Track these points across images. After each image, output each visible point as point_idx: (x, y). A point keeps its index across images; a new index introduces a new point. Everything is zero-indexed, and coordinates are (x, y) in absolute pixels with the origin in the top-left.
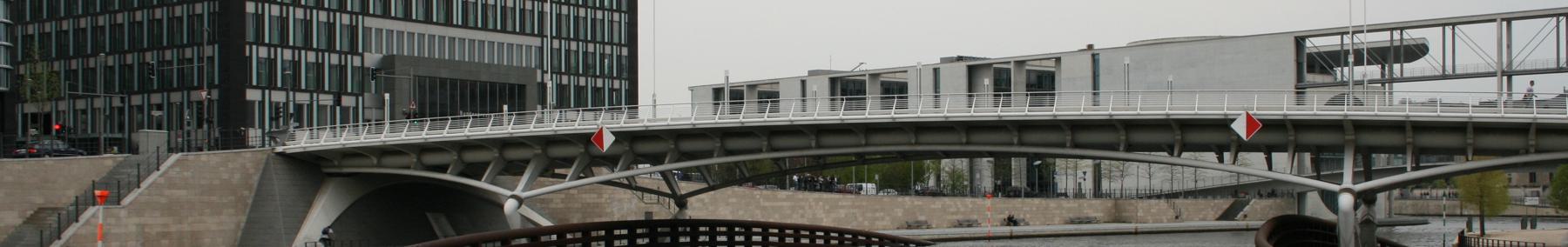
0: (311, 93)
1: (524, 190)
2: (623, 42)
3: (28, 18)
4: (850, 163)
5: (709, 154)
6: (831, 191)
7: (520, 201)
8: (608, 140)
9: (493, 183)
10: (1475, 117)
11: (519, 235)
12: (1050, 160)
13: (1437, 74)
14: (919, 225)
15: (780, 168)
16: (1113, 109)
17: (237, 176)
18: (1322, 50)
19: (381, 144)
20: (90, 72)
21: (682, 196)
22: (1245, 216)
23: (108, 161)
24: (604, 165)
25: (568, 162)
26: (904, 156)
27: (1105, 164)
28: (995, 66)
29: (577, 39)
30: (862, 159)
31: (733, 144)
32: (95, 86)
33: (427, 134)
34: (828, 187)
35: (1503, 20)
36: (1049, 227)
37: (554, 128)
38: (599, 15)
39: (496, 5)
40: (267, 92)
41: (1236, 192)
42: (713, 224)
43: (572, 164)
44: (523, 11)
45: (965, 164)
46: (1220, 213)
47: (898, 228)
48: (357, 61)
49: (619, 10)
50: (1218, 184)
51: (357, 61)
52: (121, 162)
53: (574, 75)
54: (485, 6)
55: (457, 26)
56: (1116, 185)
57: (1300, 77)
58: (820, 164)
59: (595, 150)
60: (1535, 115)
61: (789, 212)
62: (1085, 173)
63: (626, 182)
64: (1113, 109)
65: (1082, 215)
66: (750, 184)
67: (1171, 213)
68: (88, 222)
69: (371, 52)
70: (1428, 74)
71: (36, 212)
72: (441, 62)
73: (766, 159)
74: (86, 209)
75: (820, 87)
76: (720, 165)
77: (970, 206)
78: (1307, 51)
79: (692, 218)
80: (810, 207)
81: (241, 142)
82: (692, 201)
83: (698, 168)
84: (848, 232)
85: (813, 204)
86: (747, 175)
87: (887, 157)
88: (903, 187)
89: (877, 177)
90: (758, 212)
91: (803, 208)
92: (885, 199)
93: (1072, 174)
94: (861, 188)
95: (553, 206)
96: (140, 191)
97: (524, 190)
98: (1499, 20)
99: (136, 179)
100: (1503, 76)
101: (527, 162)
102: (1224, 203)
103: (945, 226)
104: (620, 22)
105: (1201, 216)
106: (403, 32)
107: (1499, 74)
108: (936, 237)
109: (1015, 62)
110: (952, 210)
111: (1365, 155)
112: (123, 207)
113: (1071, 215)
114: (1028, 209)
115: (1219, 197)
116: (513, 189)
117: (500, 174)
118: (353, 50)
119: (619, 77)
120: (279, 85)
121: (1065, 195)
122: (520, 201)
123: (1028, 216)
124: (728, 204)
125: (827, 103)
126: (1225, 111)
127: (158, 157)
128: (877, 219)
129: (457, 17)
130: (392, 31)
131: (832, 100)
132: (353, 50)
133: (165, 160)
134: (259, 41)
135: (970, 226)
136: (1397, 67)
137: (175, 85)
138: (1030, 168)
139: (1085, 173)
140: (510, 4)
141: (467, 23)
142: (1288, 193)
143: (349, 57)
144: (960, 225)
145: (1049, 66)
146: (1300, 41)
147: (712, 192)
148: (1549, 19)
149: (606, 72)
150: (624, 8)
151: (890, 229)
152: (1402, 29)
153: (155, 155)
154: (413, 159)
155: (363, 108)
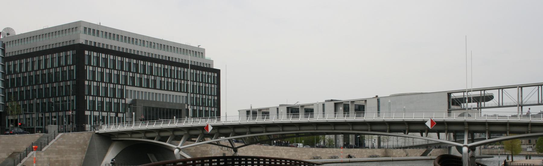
0: (108, 112)
1: (181, 146)
2: (215, 95)
3: (10, 87)
4: (294, 136)
5: (245, 134)
6: (287, 146)
7: (180, 150)
8: (210, 128)
9: (170, 143)
11: (179, 161)
12: (363, 135)
13: (497, 106)
14: (317, 158)
17: (82, 141)
20: (31, 105)
21: (236, 148)
22: (430, 155)
23: (37, 136)
24: (209, 137)
25: (196, 136)
26: (313, 134)
27: (382, 137)
28: (344, 103)
30: (298, 135)
32: (33, 110)
34: (286, 145)
35: (519, 87)
36: (362, 159)
38: (207, 85)
40: (92, 112)
41: (427, 147)
42: (246, 158)
45: (333, 137)
46: (422, 154)
48: (123, 101)
49: (214, 84)
50: (421, 144)
51: (123, 101)
52: (42, 136)
53: (198, 106)
55: (158, 89)
56: (386, 144)
58: (283, 137)
59: (206, 132)
62: (375, 140)
63: (216, 143)
65: (374, 155)
66: (259, 144)
67: (405, 154)
68: (30, 157)
69: (128, 98)
72: (152, 101)
74: (30, 152)
76: (249, 137)
78: (452, 98)
80: (280, 152)
81: (83, 129)
82: (239, 149)
84: (293, 160)
86: (258, 141)
87: (306, 134)
88: (312, 145)
89: (303, 141)
90: (262, 153)
91: (277, 152)
93: (371, 140)
94: (297, 145)
95: (191, 151)
96: (48, 146)
97: (181, 146)
98: (518, 87)
100: (519, 106)
101: (182, 136)
102: (423, 150)
103: (327, 158)
104: (214, 88)
105: (415, 155)
106: (139, 91)
107: (518, 106)
108: (323, 162)
110: (329, 153)
112: (43, 152)
114: (355, 152)
115: (421, 148)
117: (173, 140)
118: (122, 98)
119: (214, 107)
120: (97, 109)
121: (368, 147)
122: (180, 150)
125: (286, 116)
127: (55, 134)
128: (303, 156)
129: (158, 86)
132: (122, 98)
133: (57, 135)
134: (90, 94)
137: (61, 110)
139: (375, 140)
141: (161, 89)
142: (445, 147)
144: (332, 158)
145: (362, 103)
146: (449, 94)
147: (246, 147)
150: (216, 83)
154: (143, 135)
155: (126, 117)
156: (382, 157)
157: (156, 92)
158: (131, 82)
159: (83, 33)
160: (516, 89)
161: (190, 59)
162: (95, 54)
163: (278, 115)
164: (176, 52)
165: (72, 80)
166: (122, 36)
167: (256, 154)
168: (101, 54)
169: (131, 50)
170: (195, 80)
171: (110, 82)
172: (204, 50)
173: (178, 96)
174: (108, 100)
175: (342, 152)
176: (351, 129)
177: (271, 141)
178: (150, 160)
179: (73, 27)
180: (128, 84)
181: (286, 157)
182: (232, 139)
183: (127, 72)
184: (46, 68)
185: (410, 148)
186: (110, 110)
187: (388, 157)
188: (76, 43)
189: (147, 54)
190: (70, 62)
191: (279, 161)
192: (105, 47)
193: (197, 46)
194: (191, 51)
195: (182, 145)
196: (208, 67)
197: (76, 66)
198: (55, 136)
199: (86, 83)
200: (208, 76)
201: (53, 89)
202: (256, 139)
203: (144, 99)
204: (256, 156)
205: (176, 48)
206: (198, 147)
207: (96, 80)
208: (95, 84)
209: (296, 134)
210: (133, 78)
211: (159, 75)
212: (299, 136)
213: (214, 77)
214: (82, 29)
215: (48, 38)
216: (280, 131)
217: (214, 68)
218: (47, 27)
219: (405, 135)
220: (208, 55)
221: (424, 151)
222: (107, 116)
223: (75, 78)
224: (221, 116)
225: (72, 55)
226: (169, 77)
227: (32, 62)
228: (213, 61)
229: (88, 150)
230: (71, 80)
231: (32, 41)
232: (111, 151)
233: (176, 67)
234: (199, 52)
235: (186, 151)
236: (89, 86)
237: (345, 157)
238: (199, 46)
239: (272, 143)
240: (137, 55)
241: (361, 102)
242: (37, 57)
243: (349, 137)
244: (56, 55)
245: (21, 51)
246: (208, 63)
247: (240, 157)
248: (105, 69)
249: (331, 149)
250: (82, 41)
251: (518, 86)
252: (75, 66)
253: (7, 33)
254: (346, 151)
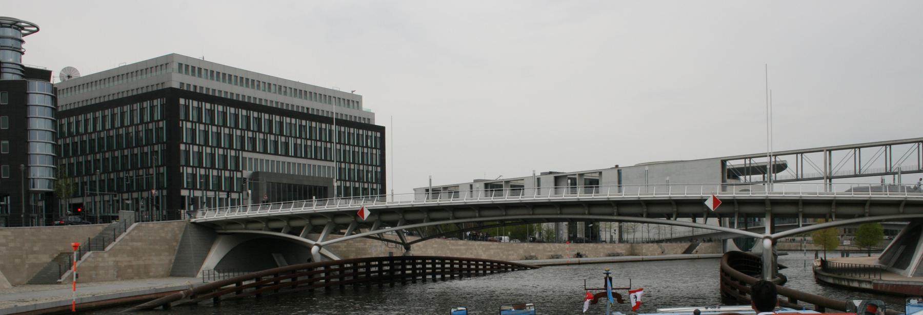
0: (215, 191)
1: (322, 241)
2: (378, 164)
3: (71, 155)
4: (495, 226)
5: (421, 221)
6: (487, 240)
7: (320, 247)
8: (367, 214)
9: (306, 237)
10: (909, 198)
11: (320, 265)
12: (597, 224)
13: (794, 178)
14: (531, 258)
15: (460, 229)
16: (640, 195)
17: (170, 235)
18: (735, 167)
19: (268, 215)
20: (93, 183)
21: (407, 243)
22: (697, 252)
23: (99, 228)
24: (366, 227)
25: (345, 226)
26: (525, 221)
27: (625, 225)
28: (568, 176)
29: (354, 163)
30: (503, 223)
31: (434, 215)
32: (105, 189)
33: (281, 211)
34: (484, 239)
35: (827, 150)
36: (598, 258)
37: (226, 216)
38: (365, 150)
41: (692, 239)
42: (424, 259)
43: (348, 227)
45: (554, 226)
46: (684, 250)
47: (521, 260)
48: (239, 175)
49: (376, 148)
50: (682, 235)
51: (239, 175)
52: (106, 228)
53: (353, 182)
55: (291, 156)
56: (631, 236)
57: (723, 181)
58: (480, 226)
59: (360, 219)
60: (906, 196)
61: (464, 251)
62: (615, 230)
64: (640, 195)
65: (615, 252)
66: (444, 237)
67: (660, 250)
68: (86, 260)
69: (246, 170)
70: (789, 178)
71: (59, 255)
72: (283, 175)
73: (452, 223)
74: (85, 253)
75: (481, 186)
76: (428, 226)
77: (558, 248)
78: (728, 167)
79: (414, 255)
80: (476, 249)
81: (178, 217)
82: (413, 246)
83: (415, 229)
84: (496, 262)
85: (477, 247)
86: (442, 232)
87: (515, 222)
88: (523, 239)
89: (509, 233)
90: (448, 252)
91: (471, 249)
92: (514, 245)
93: (608, 230)
94: (501, 239)
95: (340, 249)
96: (115, 243)
97: (322, 241)
98: (825, 151)
99: (113, 237)
100: (827, 179)
102: (686, 245)
103: (545, 258)
104: (376, 154)
105: (675, 252)
106: (263, 160)
107: (825, 178)
108: (540, 264)
109: (579, 174)
110: (549, 250)
111: (774, 217)
112: (106, 252)
113: (609, 252)
114: (587, 249)
115: (683, 242)
116: (316, 241)
117: (310, 233)
118: (237, 169)
119: (376, 183)
120: (198, 187)
121: (605, 241)
122: (320, 247)
123: (587, 252)
124: (433, 248)
125: (483, 193)
126: (702, 195)
127: (125, 224)
128: (509, 255)
129: (291, 152)
131: (486, 191)
132: (237, 169)
133: (129, 226)
134: (188, 165)
135: (557, 258)
136: (748, 177)
137: (145, 188)
138: (587, 228)
139: (615, 230)
141: (307, 156)
142: (718, 240)
144: (552, 257)
145: (596, 177)
146: (723, 162)
147: (424, 242)
148: (882, 147)
149: (369, 180)
150: (378, 147)
151: (517, 260)
152: (750, 158)
153: (124, 224)
154: (264, 225)
155: (243, 199)
156: (626, 255)
157: (250, 157)
158: (250, 145)
159: (178, 72)
160: (823, 153)
161: (334, 110)
162: (195, 104)
163: (471, 191)
164: (323, 101)
165: (161, 144)
166: (237, 77)
167: (439, 252)
168: (284, 118)
169: (249, 97)
170: (328, 140)
171: (219, 146)
172: (361, 97)
173: (322, 167)
174: (227, 174)
175: (567, 249)
176: (587, 212)
177: (463, 232)
178: (274, 261)
179: (163, 64)
180: (246, 149)
181: (484, 257)
182: (401, 230)
183: (196, 123)
184: (122, 125)
185: (666, 242)
186: (194, 186)
187: (636, 255)
188: (166, 87)
189: (274, 103)
190: (157, 115)
191: (474, 263)
192: (235, 98)
193: (351, 92)
194: (341, 99)
195: (325, 239)
196: (366, 122)
197: (166, 122)
198: (127, 227)
199: (182, 147)
200: (367, 136)
201: (143, 156)
202: (439, 230)
203: (270, 171)
204: (439, 255)
205: (327, 96)
206: (351, 243)
207: (235, 148)
208: (196, 148)
209: (501, 221)
210: (253, 140)
211: (293, 135)
212: (505, 225)
213: (376, 137)
214: (176, 66)
215: (125, 80)
216: (475, 217)
217: (376, 124)
218: (124, 64)
219: (669, 221)
220: (367, 105)
221: (687, 247)
222: (214, 196)
223: (165, 140)
224: (387, 194)
225: (161, 105)
226: (347, 143)
227: (102, 116)
228: (374, 114)
229: (179, 249)
230: (149, 145)
231: (102, 86)
232: (216, 249)
233: (318, 123)
234: (354, 101)
235: (333, 249)
236: (187, 152)
237: (572, 256)
238: (353, 92)
239: (464, 236)
240: (186, 91)
241: (593, 175)
242: (110, 110)
243: (577, 227)
244: (137, 106)
245: (87, 100)
246: (366, 117)
247: (414, 259)
248: (234, 130)
249: (552, 245)
250: (176, 85)
251: (825, 149)
252: (165, 122)
253: (67, 75)
254: (574, 247)
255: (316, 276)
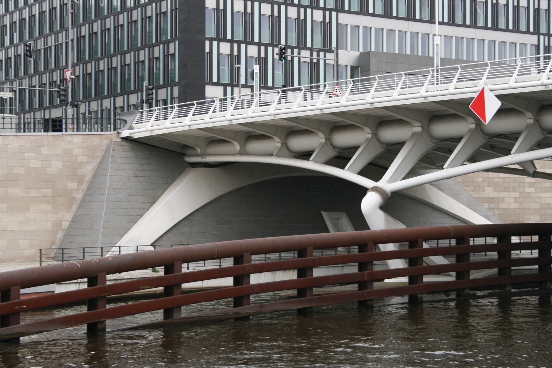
39: (507, 5)
40: (229, 89)
44: (537, 11)
54: (495, 6)
63: (517, 167)
95: (503, 206)
118: (327, 48)
130: (371, 28)
134: (220, 38)
140: (523, 3)
143: (296, 51)
154: (276, 144)
203: (397, 52)
235: (486, 205)
255: (378, 267)
